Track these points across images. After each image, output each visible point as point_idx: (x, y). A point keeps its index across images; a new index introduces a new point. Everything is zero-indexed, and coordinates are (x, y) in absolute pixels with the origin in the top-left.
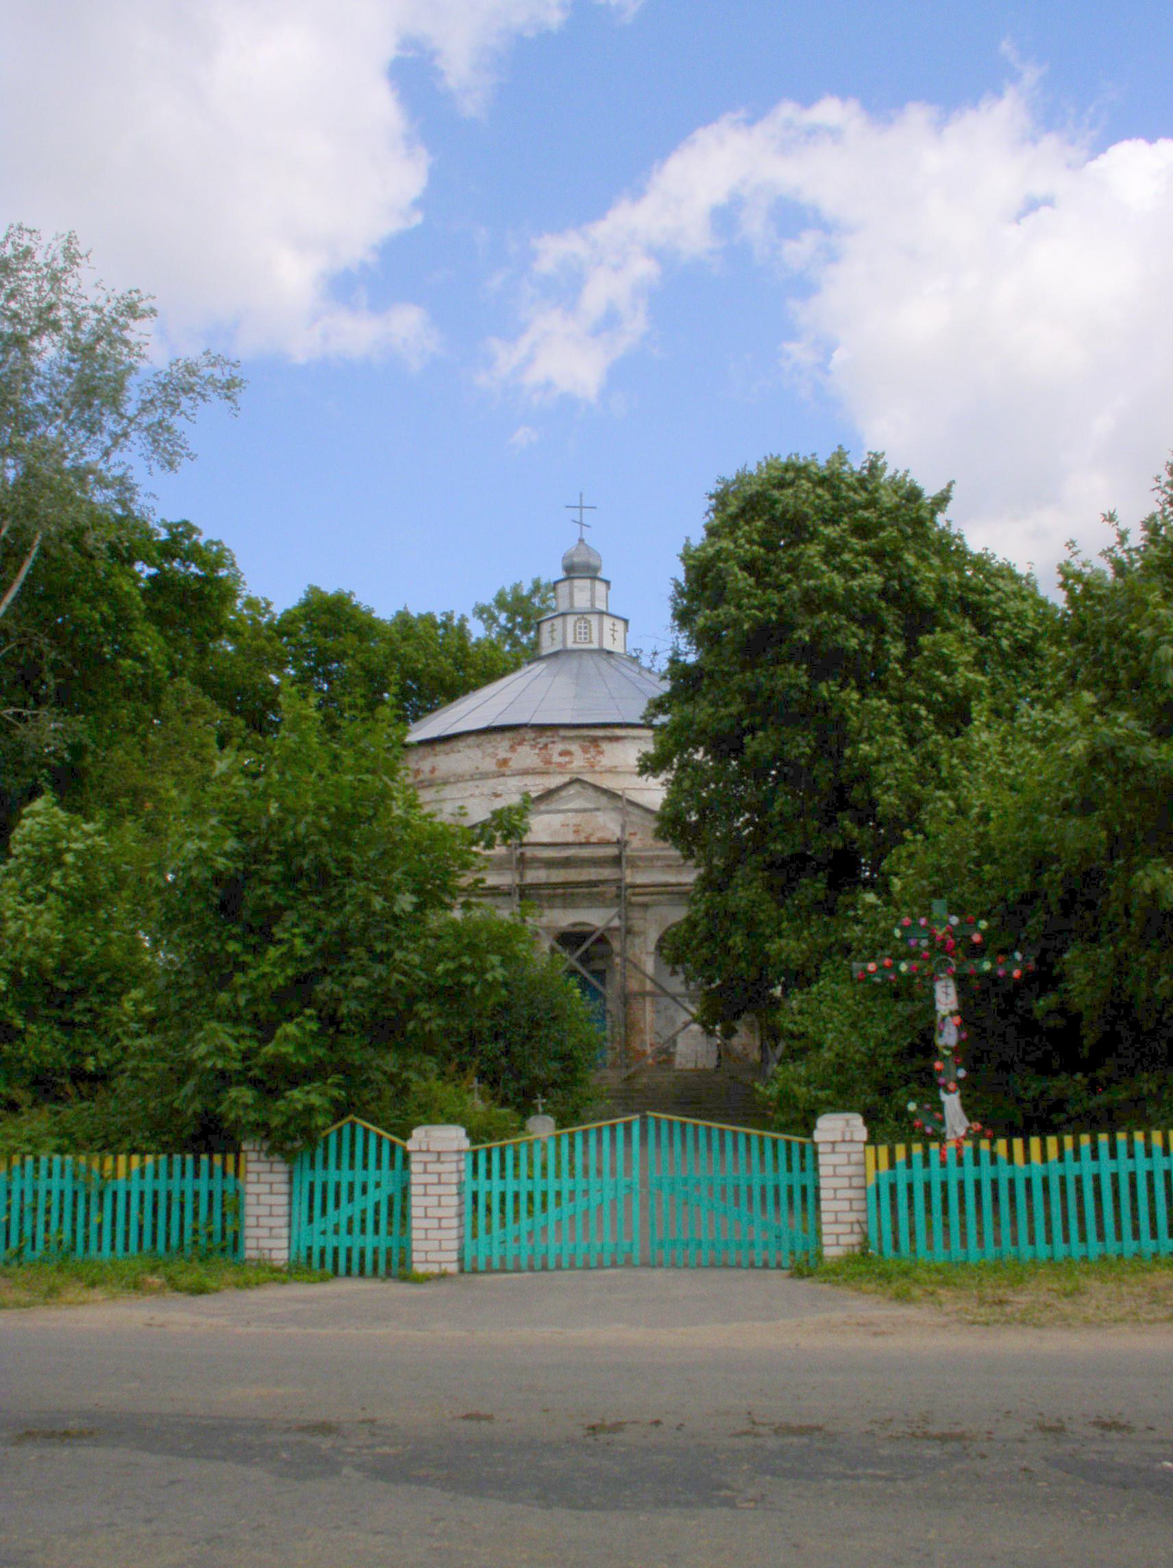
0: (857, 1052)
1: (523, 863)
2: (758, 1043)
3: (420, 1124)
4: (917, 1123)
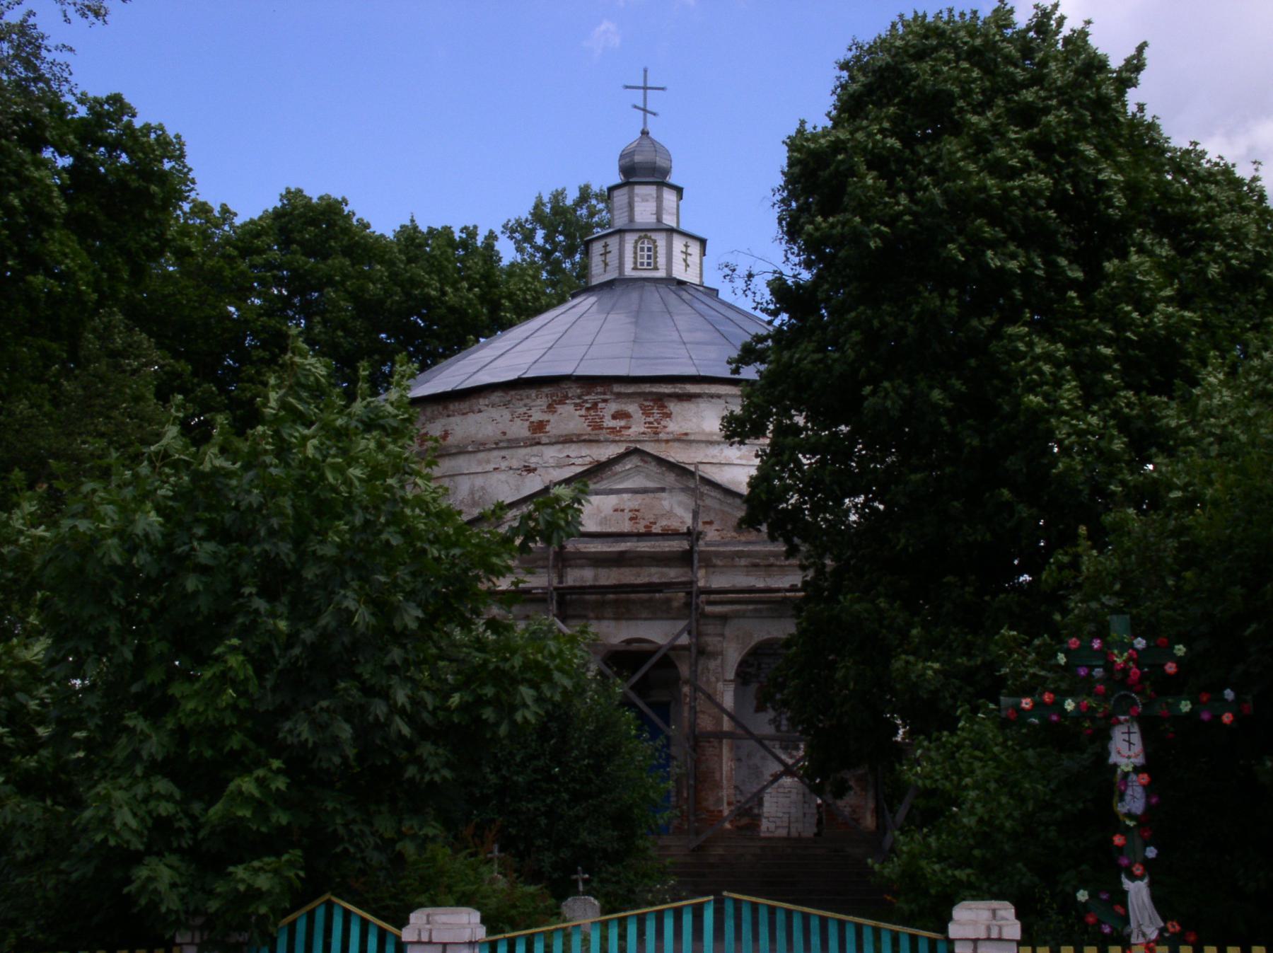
0: (1009, 816)
1: (563, 560)
2: (871, 805)
3: (421, 905)
4: (1091, 919)
